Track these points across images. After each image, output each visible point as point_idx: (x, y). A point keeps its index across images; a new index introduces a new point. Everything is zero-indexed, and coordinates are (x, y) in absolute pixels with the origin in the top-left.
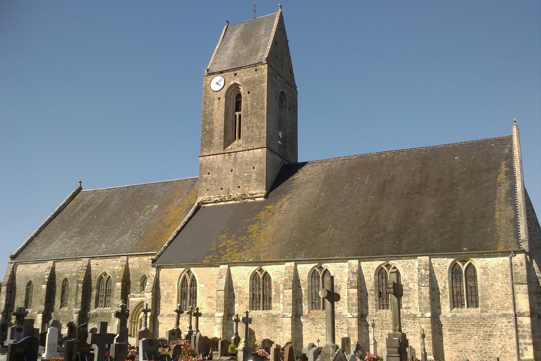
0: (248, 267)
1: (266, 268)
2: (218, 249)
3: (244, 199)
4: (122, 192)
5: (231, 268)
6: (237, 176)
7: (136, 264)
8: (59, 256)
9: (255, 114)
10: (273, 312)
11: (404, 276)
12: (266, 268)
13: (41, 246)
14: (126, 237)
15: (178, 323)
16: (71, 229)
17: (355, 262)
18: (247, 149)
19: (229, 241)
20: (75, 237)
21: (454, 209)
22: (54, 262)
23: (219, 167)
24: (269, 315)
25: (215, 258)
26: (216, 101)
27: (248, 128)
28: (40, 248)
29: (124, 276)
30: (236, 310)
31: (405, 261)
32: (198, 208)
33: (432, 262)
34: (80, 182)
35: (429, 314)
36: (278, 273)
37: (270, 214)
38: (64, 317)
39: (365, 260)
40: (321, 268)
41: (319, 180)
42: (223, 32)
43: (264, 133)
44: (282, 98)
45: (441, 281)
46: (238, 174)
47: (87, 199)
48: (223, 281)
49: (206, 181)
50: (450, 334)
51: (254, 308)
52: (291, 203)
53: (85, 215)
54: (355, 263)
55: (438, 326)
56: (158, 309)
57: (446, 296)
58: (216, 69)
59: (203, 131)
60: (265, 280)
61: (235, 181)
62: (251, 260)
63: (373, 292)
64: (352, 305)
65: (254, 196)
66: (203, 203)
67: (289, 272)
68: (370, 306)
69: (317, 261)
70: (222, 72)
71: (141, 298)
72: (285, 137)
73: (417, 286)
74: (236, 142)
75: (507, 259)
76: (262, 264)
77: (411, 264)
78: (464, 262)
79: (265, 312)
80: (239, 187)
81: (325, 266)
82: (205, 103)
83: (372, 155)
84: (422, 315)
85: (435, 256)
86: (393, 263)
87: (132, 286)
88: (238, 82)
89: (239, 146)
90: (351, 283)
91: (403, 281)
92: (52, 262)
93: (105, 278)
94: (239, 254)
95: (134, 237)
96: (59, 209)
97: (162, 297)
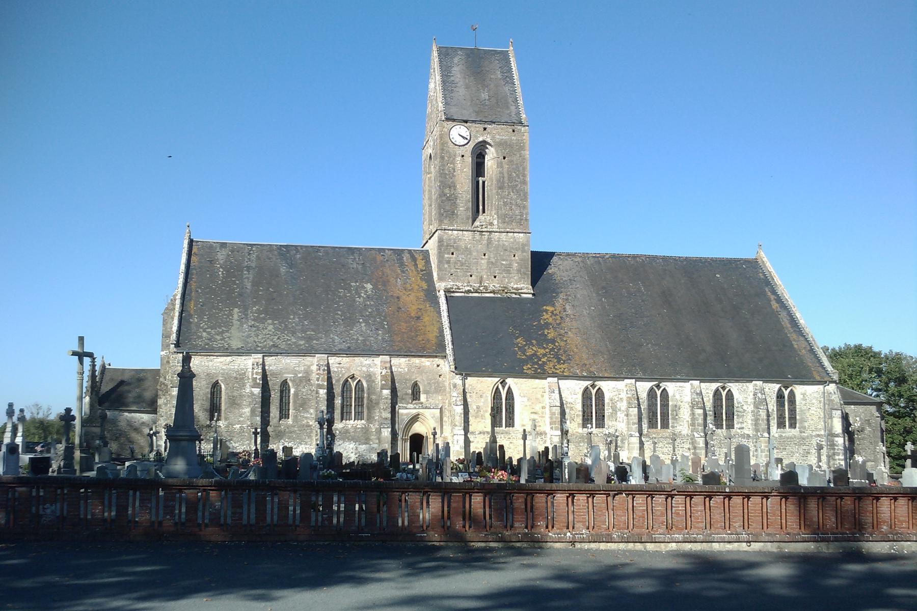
23: (466, 248)
26: (459, 158)
46: (493, 260)
49: (448, 262)
75: (821, 387)
78: (786, 388)
88: (489, 140)
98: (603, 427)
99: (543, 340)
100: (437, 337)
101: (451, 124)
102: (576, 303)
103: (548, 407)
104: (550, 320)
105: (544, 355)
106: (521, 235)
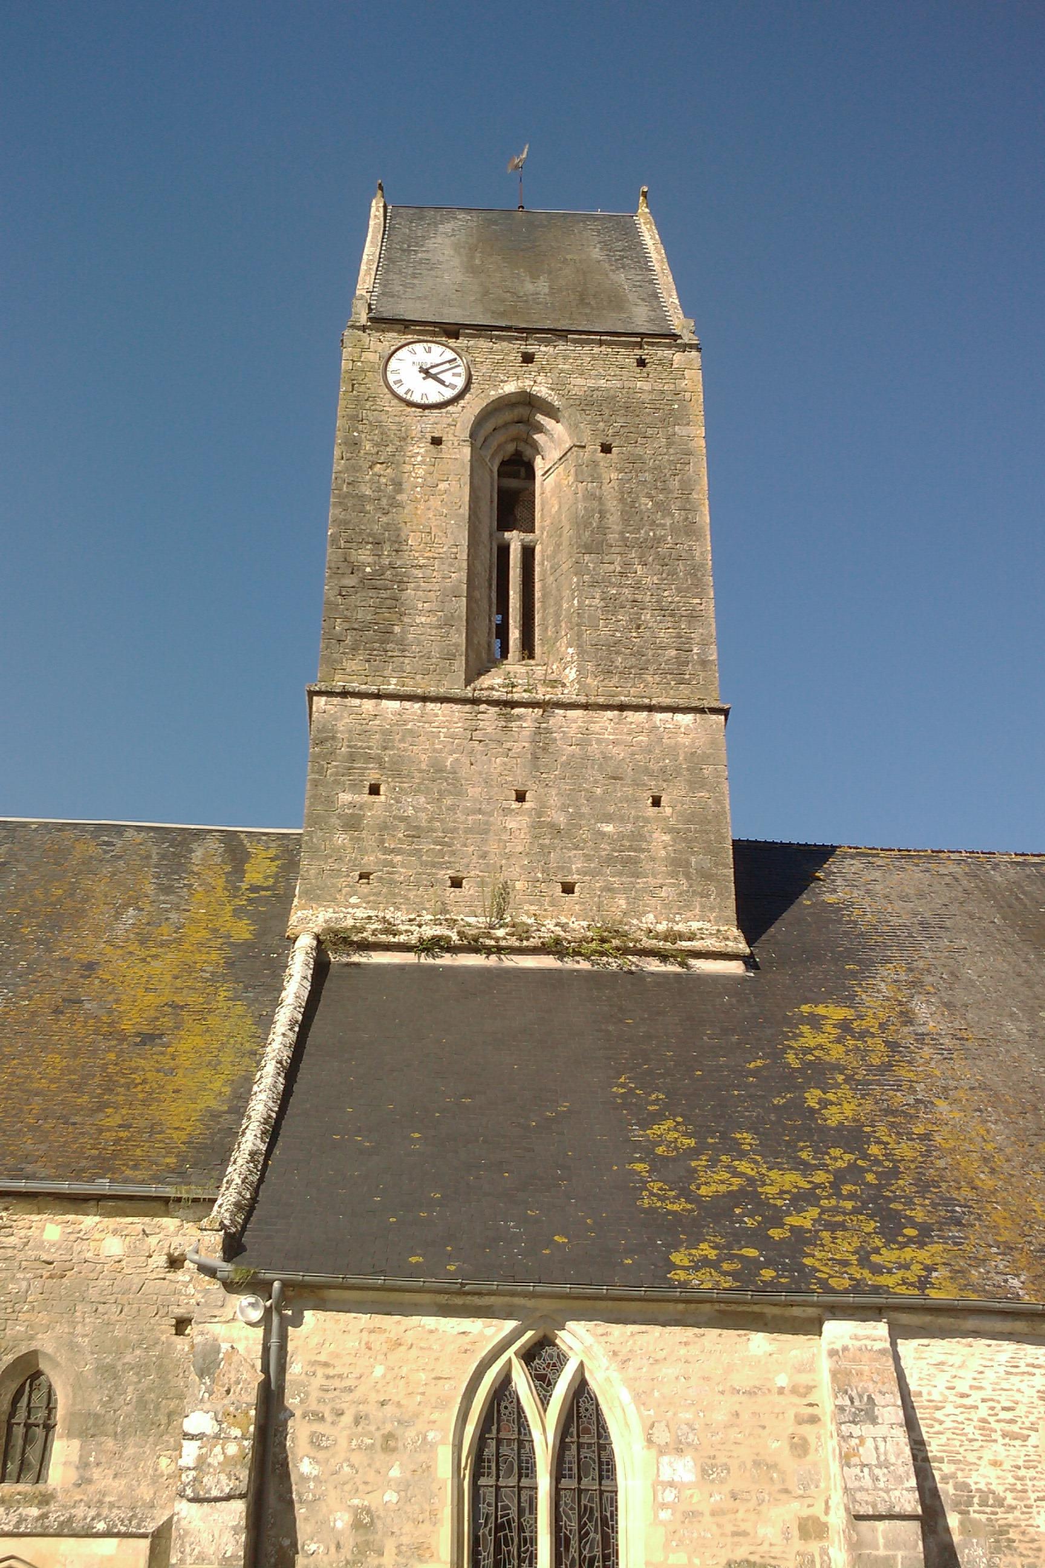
0: (378, 1320)
18: (616, 700)
23: (438, 768)
26: (420, 449)
46: (561, 819)
49: (352, 823)
61: (545, 851)
65: (685, 944)
88: (542, 390)
99: (792, 1132)
100: (215, 1115)
101: (392, 338)
102: (961, 996)
103: (837, 1519)
104: (837, 1053)
105: (801, 1199)
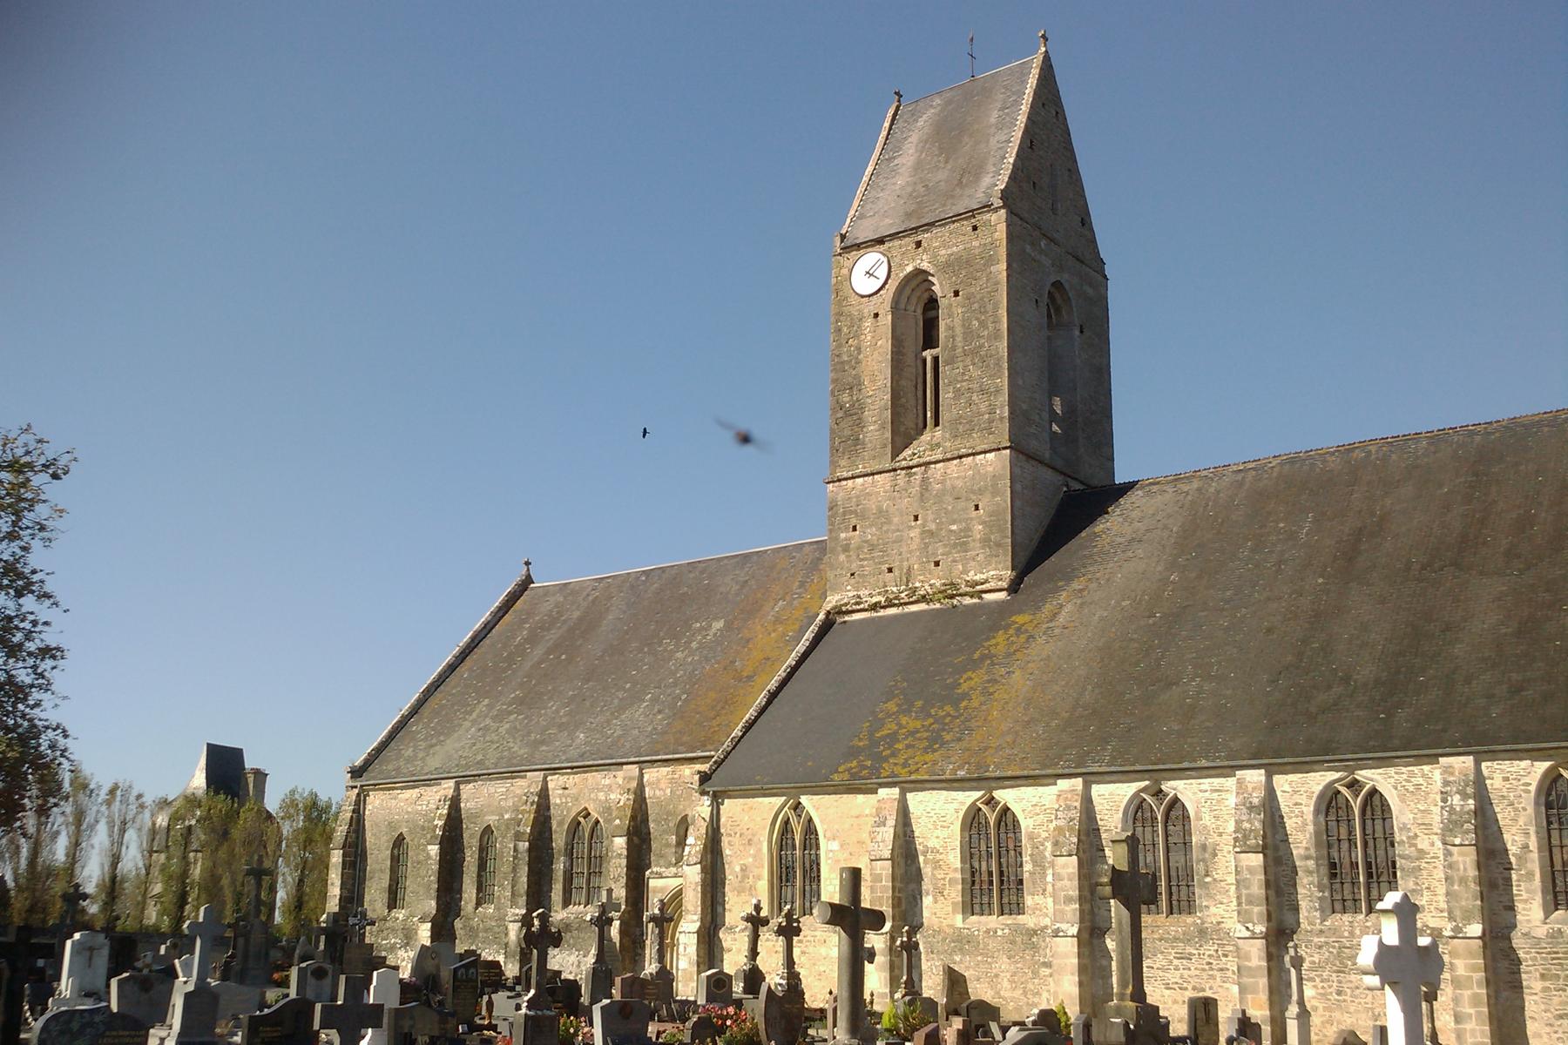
1: (1005, 796)
2: (874, 743)
3: (952, 597)
4: (632, 587)
5: (909, 796)
6: (931, 533)
7: (663, 786)
8: (467, 767)
9: (974, 352)
10: (1028, 920)
11: (1402, 815)
12: (1005, 796)
13: (425, 739)
14: (638, 713)
15: (754, 953)
16: (501, 693)
17: (1255, 777)
18: (956, 453)
19: (904, 720)
20: (510, 713)
21: (1561, 609)
22: (457, 784)
23: (880, 510)
24: (1016, 929)
25: (866, 767)
27: (958, 394)
28: (423, 745)
29: (633, 818)
30: (926, 914)
31: (1404, 769)
32: (827, 625)
33: (1485, 772)
34: (527, 563)
35: (1476, 929)
36: (1038, 808)
37: (1023, 637)
38: (486, 930)
39: (1285, 769)
40: (1159, 794)
41: (1166, 534)
42: (887, 125)
43: (1002, 407)
44: (1059, 301)
45: (1514, 830)
46: (933, 527)
47: (546, 607)
48: (888, 833)
49: (846, 549)
50: (1546, 989)
51: (977, 908)
52: (1082, 604)
53: (539, 652)
54: (1255, 779)
55: (1506, 963)
56: (720, 909)
57: (1530, 874)
58: (865, 233)
59: (833, 409)
60: (1002, 830)
61: (927, 546)
62: (961, 773)
63: (1311, 863)
64: (1250, 903)
66: (841, 613)
67: (1068, 808)
68: (1304, 905)
69: (1147, 775)
70: (880, 241)
71: (674, 879)
72: (1070, 409)
73: (1439, 844)
74: (926, 437)
76: (994, 784)
77: (1421, 781)
79: (1007, 920)
80: (937, 564)
81: (1172, 787)
82: (839, 330)
83: (1323, 455)
84: (1457, 929)
85: (1493, 756)
86: (1371, 777)
87: (654, 846)
88: (925, 266)
89: (934, 447)
90: (1246, 837)
91: (1401, 829)
92: (451, 783)
93: (586, 826)
94: (929, 757)
95: (659, 712)
96: (473, 639)
97: (729, 877)
98: (1021, 911)
106: (991, 456)
